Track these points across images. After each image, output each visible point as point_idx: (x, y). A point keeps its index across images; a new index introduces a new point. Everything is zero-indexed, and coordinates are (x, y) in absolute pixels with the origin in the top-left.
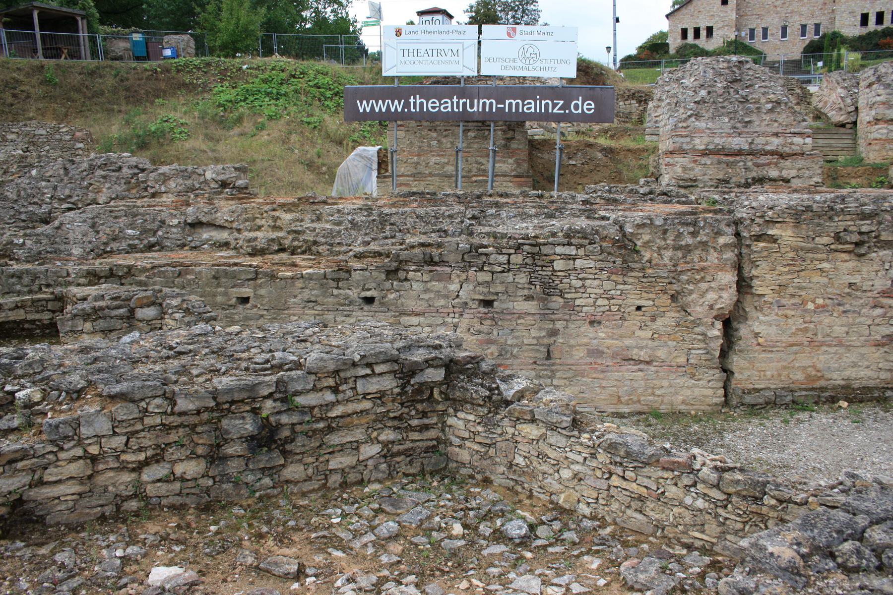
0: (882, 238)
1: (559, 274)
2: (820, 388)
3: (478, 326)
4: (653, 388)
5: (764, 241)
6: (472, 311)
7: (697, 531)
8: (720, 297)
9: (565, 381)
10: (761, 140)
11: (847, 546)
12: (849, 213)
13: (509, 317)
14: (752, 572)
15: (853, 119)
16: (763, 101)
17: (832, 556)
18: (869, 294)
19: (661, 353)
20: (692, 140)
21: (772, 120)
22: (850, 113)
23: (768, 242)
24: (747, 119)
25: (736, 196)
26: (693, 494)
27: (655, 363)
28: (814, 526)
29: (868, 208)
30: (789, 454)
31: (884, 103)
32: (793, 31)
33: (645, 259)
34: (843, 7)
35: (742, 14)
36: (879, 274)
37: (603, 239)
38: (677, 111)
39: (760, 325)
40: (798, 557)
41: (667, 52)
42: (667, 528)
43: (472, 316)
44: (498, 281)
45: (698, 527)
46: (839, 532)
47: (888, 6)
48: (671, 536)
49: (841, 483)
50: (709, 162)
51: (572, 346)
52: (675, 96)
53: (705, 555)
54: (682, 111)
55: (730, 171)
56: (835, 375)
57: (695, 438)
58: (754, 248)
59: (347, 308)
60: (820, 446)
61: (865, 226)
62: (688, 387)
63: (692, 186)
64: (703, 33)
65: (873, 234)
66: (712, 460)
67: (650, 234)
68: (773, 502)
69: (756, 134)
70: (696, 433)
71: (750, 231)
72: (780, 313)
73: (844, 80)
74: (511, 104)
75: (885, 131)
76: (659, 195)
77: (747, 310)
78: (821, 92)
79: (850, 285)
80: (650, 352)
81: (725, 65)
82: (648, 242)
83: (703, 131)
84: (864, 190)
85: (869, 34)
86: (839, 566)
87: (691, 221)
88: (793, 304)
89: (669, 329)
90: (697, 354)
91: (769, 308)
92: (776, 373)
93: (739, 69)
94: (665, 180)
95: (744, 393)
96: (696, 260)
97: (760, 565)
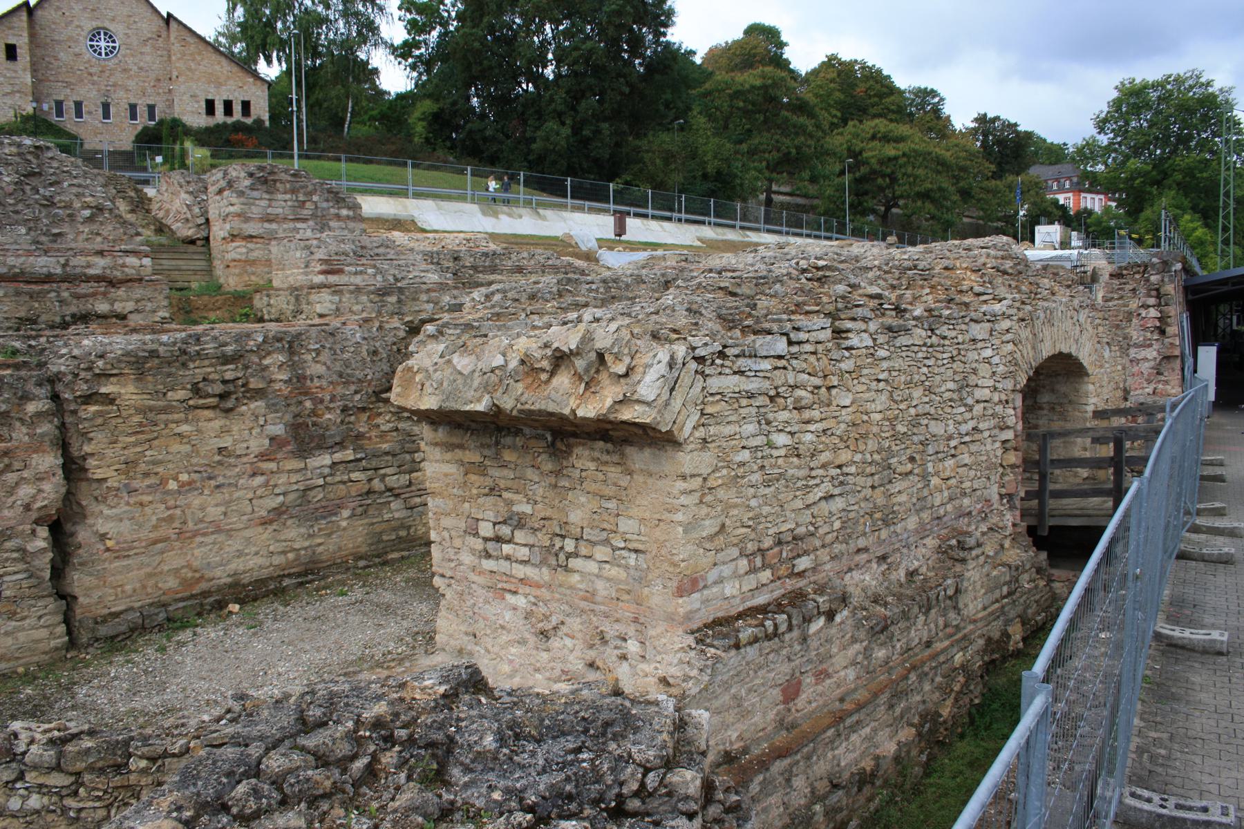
0: (251, 386)
2: (201, 594)
5: (96, 402)
8: (40, 491)
10: (79, 261)
11: (242, 788)
12: (207, 357)
15: (204, 234)
16: (77, 205)
17: (225, 808)
18: (245, 460)
21: (92, 233)
22: (199, 225)
23: (102, 403)
24: (56, 231)
25: (48, 342)
26: (22, 792)
28: (197, 777)
29: (229, 349)
31: (239, 215)
32: (119, 110)
34: (183, 88)
35: (40, 77)
36: (254, 432)
39: (106, 522)
46: (229, 774)
47: (236, 94)
55: (37, 305)
56: (218, 572)
57: (29, 707)
58: (83, 415)
60: (212, 671)
61: (229, 373)
65: (240, 382)
66: (45, 731)
68: (143, 764)
69: (71, 253)
70: (29, 699)
72: (132, 501)
73: (188, 182)
75: (244, 250)
77: (84, 503)
78: (160, 197)
81: (14, 149)
84: (223, 325)
85: (218, 126)
86: (235, 818)
88: (149, 487)
91: (116, 496)
92: (138, 585)
93: (37, 157)
95: (97, 623)
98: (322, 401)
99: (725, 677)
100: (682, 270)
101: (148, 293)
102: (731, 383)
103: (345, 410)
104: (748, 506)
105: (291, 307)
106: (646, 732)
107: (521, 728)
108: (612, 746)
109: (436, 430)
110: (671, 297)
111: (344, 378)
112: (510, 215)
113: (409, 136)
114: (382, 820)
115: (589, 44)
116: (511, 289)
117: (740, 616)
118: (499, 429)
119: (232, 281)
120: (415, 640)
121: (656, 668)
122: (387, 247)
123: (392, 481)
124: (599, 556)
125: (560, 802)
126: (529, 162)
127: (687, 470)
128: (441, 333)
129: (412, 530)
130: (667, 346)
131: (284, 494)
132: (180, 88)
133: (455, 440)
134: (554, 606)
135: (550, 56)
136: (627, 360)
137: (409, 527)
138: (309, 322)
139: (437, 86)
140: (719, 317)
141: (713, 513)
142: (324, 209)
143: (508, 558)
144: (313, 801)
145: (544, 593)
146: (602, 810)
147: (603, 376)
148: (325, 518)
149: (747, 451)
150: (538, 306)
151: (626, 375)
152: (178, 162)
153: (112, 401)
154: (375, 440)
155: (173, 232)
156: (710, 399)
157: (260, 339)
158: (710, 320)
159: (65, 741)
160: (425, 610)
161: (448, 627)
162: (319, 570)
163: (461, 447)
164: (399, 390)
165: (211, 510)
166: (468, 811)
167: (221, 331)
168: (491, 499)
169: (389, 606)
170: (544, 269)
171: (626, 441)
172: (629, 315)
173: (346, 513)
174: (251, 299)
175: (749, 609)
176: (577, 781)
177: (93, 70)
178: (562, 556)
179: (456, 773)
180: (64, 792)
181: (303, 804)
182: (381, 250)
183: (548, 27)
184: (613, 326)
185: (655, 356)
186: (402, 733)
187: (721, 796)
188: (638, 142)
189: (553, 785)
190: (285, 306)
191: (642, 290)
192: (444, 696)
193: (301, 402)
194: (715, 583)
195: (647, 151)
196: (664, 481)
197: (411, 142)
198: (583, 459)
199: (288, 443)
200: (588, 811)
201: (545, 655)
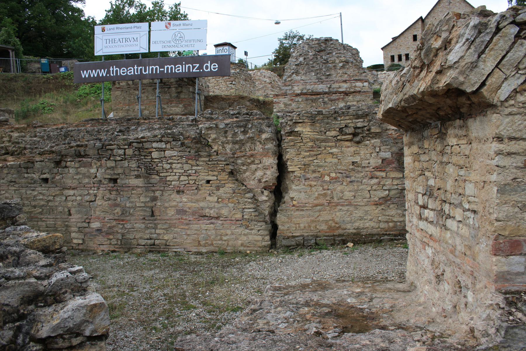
0: (372, 131)
1: (155, 160)
3: (108, 196)
4: (221, 235)
6: (104, 186)
9: (164, 231)
10: (336, 85)
13: (126, 189)
16: (337, 61)
18: (367, 169)
19: (225, 212)
20: (292, 87)
27: (221, 219)
37: (186, 138)
39: (295, 192)
43: (105, 189)
44: (119, 166)
50: (300, 100)
51: (167, 208)
56: (348, 226)
59: (33, 185)
62: (244, 234)
64: (404, 58)
67: (216, 133)
69: (333, 82)
74: (168, 68)
79: (353, 163)
83: (299, 82)
88: (315, 178)
89: (228, 195)
91: (299, 180)
92: (307, 225)
93: (326, 44)
96: (247, 150)
199: (393, 163)
201: (437, 294)
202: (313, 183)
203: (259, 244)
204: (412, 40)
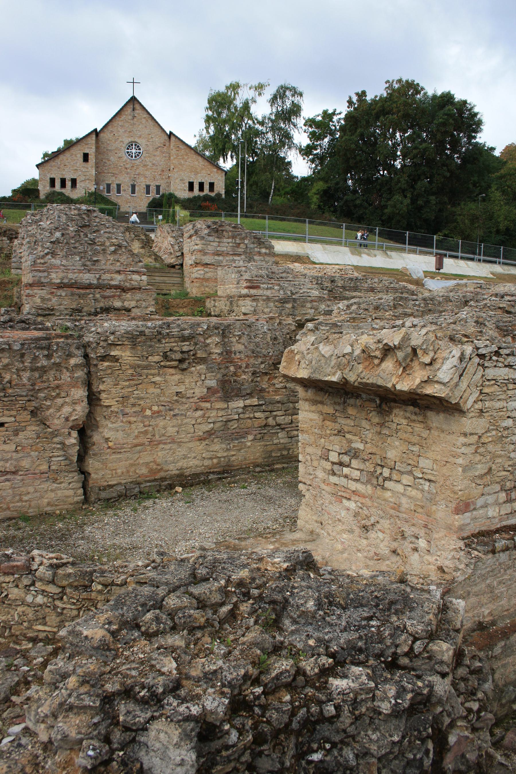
0: (198, 356)
4: (20, 495)
5: (108, 361)
7: (40, 624)
8: (74, 410)
11: (149, 616)
12: (173, 337)
14: (71, 657)
15: (180, 262)
17: (138, 627)
18: (192, 400)
19: (25, 463)
23: (111, 361)
25: (86, 323)
26: (33, 592)
27: (20, 473)
28: (124, 604)
29: (187, 333)
30: (138, 537)
31: (200, 251)
32: (140, 189)
33: (6, 380)
34: (176, 175)
35: (100, 170)
38: (36, 249)
39: (110, 431)
40: (109, 634)
41: (38, 197)
42: (13, 627)
45: (41, 621)
46: (143, 605)
48: (18, 633)
49: (154, 561)
50: (63, 294)
52: (33, 236)
53: (48, 644)
54: (40, 249)
56: (171, 467)
57: (60, 534)
58: (100, 367)
60: (161, 526)
62: (52, 491)
63: (49, 315)
64: (69, 184)
65: (192, 353)
67: (9, 358)
68: (100, 587)
70: (60, 530)
71: (96, 353)
72: (125, 420)
76: (18, 322)
77: (98, 419)
80: (15, 463)
81: (76, 212)
82: (8, 365)
83: (58, 267)
85: (195, 197)
86: (143, 634)
87: (45, 345)
88: (135, 412)
89: (31, 441)
90: (58, 460)
92: (125, 470)
93: (88, 216)
94: (26, 309)
96: (51, 379)
97: (77, 649)
98: (240, 367)
99: (483, 572)
100: (477, 294)
101: (144, 296)
102: (502, 373)
103: (254, 373)
104: (509, 457)
105: (227, 308)
106: (418, 612)
107: (333, 598)
108: (394, 618)
109: (307, 391)
110: (465, 313)
111: (255, 353)
112: (368, 255)
113: (308, 204)
114: (235, 648)
115: (424, 145)
116: (363, 303)
117: (497, 531)
118: (346, 393)
119: (194, 291)
120: (285, 522)
121: (437, 560)
122: (288, 273)
123: (280, 420)
124: (405, 482)
125: (353, 653)
126: (382, 221)
127: (468, 430)
128: (317, 329)
129: (291, 451)
130: (459, 346)
131: (214, 423)
132: (174, 175)
133: (319, 398)
134: (373, 510)
135: (399, 153)
136: (431, 354)
137: (290, 449)
138: (237, 318)
139: (327, 173)
140: (497, 327)
141: (484, 460)
142: (251, 248)
143: (346, 476)
144: (192, 630)
145: (368, 502)
146: (382, 662)
147: (415, 364)
148: (237, 439)
149: (511, 420)
150: (380, 314)
151: (431, 364)
152: (170, 218)
153: (117, 360)
154: (272, 393)
155: (163, 260)
156: (487, 383)
157: (205, 327)
158: (491, 329)
159: (58, 566)
160: (293, 503)
161: (305, 516)
162: (231, 471)
163: (322, 403)
164: (285, 364)
165: (169, 429)
166: (291, 650)
167: (184, 321)
168: (338, 438)
169: (271, 498)
170: (387, 290)
171: (428, 408)
172: (436, 324)
173: (250, 437)
174: (204, 302)
175: (505, 527)
176: (366, 640)
177: (127, 166)
178: (381, 479)
179: (287, 622)
180: (55, 597)
181: (185, 631)
182: (284, 275)
183: (398, 135)
184: (424, 331)
185: (451, 352)
186: (255, 592)
187: (468, 662)
188: (454, 209)
189: (349, 641)
190: (224, 307)
191: (449, 306)
192: (286, 570)
193: (227, 367)
194: (482, 507)
195: (460, 215)
196: (451, 436)
197: (309, 207)
198: (399, 418)
199: (218, 392)
200: (371, 662)
201: (365, 542)
202: (133, 419)
203: (70, 500)
204: (82, 159)
